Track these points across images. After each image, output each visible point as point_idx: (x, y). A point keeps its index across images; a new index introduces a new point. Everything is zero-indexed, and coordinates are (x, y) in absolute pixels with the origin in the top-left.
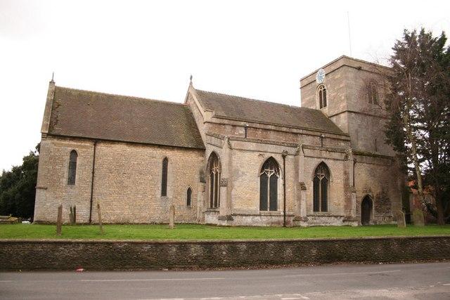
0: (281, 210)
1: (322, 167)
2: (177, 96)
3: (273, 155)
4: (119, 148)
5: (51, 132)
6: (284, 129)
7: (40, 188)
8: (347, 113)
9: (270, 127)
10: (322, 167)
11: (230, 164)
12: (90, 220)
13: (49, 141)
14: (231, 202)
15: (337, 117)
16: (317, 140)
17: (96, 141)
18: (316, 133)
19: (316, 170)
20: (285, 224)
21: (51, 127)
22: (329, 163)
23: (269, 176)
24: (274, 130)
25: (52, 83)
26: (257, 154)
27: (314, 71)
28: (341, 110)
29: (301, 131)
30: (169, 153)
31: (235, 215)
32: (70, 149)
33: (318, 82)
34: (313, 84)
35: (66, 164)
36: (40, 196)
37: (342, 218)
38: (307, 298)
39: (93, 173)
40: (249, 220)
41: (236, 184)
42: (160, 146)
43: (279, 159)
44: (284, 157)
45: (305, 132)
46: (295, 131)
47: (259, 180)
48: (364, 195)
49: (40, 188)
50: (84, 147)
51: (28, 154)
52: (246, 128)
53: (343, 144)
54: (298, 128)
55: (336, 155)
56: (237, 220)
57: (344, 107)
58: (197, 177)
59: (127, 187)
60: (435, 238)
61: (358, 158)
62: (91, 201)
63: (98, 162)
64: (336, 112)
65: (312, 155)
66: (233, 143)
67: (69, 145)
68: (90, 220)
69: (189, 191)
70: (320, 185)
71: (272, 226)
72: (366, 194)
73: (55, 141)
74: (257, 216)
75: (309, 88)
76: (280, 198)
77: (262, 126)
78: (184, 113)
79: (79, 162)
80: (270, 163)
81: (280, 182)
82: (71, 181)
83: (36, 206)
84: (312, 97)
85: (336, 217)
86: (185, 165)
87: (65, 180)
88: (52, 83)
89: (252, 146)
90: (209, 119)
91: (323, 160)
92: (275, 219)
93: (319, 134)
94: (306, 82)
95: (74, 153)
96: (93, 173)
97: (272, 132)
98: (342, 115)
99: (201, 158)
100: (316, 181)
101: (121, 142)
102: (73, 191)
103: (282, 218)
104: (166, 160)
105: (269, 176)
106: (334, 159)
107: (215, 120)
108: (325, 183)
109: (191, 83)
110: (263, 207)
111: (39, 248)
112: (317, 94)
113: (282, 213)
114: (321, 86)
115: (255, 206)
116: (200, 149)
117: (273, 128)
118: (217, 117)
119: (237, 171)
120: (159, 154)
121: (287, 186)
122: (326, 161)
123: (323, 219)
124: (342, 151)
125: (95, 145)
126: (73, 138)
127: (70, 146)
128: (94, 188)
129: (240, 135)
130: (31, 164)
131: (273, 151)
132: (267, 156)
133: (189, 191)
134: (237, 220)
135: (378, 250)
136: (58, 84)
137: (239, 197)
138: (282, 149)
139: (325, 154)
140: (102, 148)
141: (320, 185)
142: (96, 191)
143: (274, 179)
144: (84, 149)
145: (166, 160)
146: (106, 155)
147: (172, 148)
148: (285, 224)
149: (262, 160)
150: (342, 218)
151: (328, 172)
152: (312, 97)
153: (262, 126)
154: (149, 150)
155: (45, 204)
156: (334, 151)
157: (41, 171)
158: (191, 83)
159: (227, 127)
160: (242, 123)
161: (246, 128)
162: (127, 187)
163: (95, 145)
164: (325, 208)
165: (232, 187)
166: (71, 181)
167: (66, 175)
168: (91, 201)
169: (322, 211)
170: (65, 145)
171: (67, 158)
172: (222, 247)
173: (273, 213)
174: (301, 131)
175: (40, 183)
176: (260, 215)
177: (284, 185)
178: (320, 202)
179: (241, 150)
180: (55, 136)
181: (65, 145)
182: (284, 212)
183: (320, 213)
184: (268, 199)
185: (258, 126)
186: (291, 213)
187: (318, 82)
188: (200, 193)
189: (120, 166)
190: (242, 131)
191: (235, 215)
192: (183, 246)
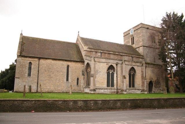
0: (115, 87)
1: (133, 69)
2: (73, 40)
3: (112, 64)
4: (49, 61)
5: (21, 54)
6: (117, 53)
7: (17, 78)
8: (142, 47)
9: (111, 52)
10: (133, 69)
11: (95, 68)
12: (37, 91)
13: (20, 58)
14: (95, 84)
15: (139, 48)
16: (131, 58)
17: (40, 58)
18: (130, 55)
19: (130, 70)
20: (117, 93)
21: (21, 53)
22: (135, 68)
23: (111, 73)
24: (113, 54)
25: (21, 34)
26: (106, 64)
27: (129, 29)
28: (140, 46)
29: (124, 54)
30: (69, 63)
31: (97, 89)
32: (29, 62)
33: (131, 34)
34: (129, 35)
35: (27, 68)
36: (16, 81)
37: (141, 90)
38: (126, 123)
39: (38, 71)
40: (102, 91)
41: (97, 76)
42: (66, 60)
43: (115, 66)
44: (117, 65)
45: (125, 54)
46: (121, 54)
47: (107, 74)
48: (150, 80)
49: (17, 78)
50: (35, 61)
51: (11, 64)
52: (101, 53)
53: (141, 59)
54: (123, 53)
55: (138, 64)
56: (97, 91)
57: (141, 44)
58: (81, 73)
59: (52, 77)
60: (179, 99)
61: (147, 65)
62: (38, 83)
63: (40, 67)
64: (138, 46)
65: (128, 64)
66: (96, 59)
67: (28, 60)
68: (37, 91)
69: (78, 79)
70: (132, 76)
71: (112, 94)
72: (150, 80)
73: (23, 58)
74: (105, 89)
75: (127, 36)
76: (115, 82)
77: (108, 52)
78: (75, 47)
79: (32, 67)
80: (111, 67)
81: (115, 75)
82: (29, 75)
83: (15, 85)
84: (128, 40)
85: (138, 90)
86: (76, 68)
87: (27, 75)
88: (21, 34)
89: (104, 60)
90: (86, 49)
91: (133, 66)
92: (113, 91)
93: (131, 55)
94: (126, 34)
95: (30, 63)
96: (38, 71)
97: (112, 55)
98: (141, 48)
99: (83, 65)
100: (130, 75)
101: (50, 59)
102: (30, 79)
103: (116, 90)
104: (68, 66)
105: (111, 73)
106: (137, 66)
107: (88, 50)
108: (134, 76)
109: (79, 34)
110: (108, 85)
111: (16, 103)
112: (131, 39)
113: (116, 88)
114: (132, 36)
115: (105, 85)
116: (82, 62)
117: (112, 53)
118: (89, 48)
119: (97, 71)
120: (66, 63)
121: (118, 77)
122: (134, 67)
123: (133, 90)
124: (141, 63)
125: (39, 60)
126: (30, 57)
127: (29, 60)
128: (39, 78)
129: (99, 56)
130: (13, 68)
131: (112, 62)
132: (110, 64)
133: (78, 79)
134: (97, 91)
135: (156, 103)
136: (24, 35)
137: (98, 82)
138: (116, 61)
139: (133, 64)
140: (42, 61)
141: (132, 76)
142: (40, 79)
143: (113, 74)
144: (35, 62)
145: (68, 66)
146: (43, 64)
147: (71, 61)
148: (117, 93)
149: (108, 66)
150: (141, 90)
151: (135, 71)
152: (128, 40)
153: (108, 52)
154: (61, 62)
155: (18, 84)
156: (137, 62)
157: (17, 71)
158: (79, 34)
159: (93, 52)
160: (100, 51)
161: (101, 53)
162: (52, 77)
163: (39, 60)
164: (133, 86)
165: (95, 77)
166: (29, 75)
167: (27, 72)
168: (38, 83)
169: (132, 87)
170: (27, 60)
171: (28, 65)
172: (91, 102)
173: (112, 88)
174: (124, 54)
175: (16, 76)
176: (107, 89)
177: (117, 76)
178: (132, 84)
179: (99, 62)
180: (22, 56)
181: (27, 60)
182: (117, 88)
183: (132, 88)
184: (110, 82)
185: (106, 52)
186: (120, 88)
187: (131, 34)
188: (82, 80)
189: (49, 69)
190: (99, 54)
191: (97, 89)
192: (75, 102)
